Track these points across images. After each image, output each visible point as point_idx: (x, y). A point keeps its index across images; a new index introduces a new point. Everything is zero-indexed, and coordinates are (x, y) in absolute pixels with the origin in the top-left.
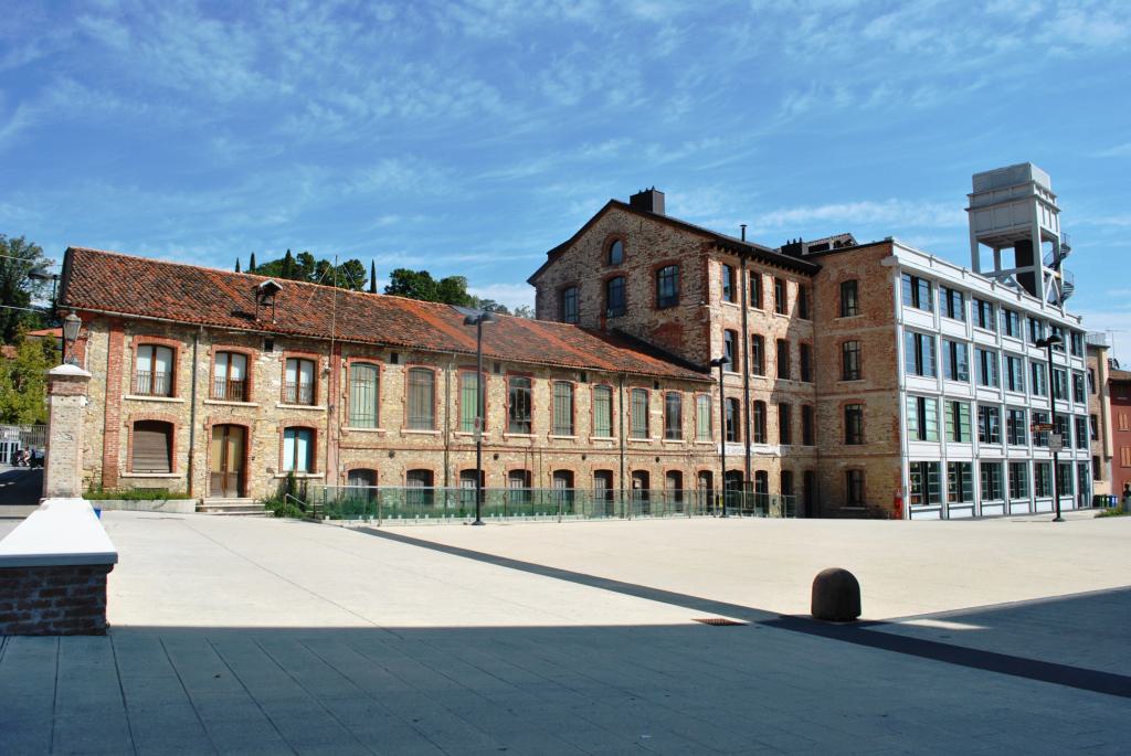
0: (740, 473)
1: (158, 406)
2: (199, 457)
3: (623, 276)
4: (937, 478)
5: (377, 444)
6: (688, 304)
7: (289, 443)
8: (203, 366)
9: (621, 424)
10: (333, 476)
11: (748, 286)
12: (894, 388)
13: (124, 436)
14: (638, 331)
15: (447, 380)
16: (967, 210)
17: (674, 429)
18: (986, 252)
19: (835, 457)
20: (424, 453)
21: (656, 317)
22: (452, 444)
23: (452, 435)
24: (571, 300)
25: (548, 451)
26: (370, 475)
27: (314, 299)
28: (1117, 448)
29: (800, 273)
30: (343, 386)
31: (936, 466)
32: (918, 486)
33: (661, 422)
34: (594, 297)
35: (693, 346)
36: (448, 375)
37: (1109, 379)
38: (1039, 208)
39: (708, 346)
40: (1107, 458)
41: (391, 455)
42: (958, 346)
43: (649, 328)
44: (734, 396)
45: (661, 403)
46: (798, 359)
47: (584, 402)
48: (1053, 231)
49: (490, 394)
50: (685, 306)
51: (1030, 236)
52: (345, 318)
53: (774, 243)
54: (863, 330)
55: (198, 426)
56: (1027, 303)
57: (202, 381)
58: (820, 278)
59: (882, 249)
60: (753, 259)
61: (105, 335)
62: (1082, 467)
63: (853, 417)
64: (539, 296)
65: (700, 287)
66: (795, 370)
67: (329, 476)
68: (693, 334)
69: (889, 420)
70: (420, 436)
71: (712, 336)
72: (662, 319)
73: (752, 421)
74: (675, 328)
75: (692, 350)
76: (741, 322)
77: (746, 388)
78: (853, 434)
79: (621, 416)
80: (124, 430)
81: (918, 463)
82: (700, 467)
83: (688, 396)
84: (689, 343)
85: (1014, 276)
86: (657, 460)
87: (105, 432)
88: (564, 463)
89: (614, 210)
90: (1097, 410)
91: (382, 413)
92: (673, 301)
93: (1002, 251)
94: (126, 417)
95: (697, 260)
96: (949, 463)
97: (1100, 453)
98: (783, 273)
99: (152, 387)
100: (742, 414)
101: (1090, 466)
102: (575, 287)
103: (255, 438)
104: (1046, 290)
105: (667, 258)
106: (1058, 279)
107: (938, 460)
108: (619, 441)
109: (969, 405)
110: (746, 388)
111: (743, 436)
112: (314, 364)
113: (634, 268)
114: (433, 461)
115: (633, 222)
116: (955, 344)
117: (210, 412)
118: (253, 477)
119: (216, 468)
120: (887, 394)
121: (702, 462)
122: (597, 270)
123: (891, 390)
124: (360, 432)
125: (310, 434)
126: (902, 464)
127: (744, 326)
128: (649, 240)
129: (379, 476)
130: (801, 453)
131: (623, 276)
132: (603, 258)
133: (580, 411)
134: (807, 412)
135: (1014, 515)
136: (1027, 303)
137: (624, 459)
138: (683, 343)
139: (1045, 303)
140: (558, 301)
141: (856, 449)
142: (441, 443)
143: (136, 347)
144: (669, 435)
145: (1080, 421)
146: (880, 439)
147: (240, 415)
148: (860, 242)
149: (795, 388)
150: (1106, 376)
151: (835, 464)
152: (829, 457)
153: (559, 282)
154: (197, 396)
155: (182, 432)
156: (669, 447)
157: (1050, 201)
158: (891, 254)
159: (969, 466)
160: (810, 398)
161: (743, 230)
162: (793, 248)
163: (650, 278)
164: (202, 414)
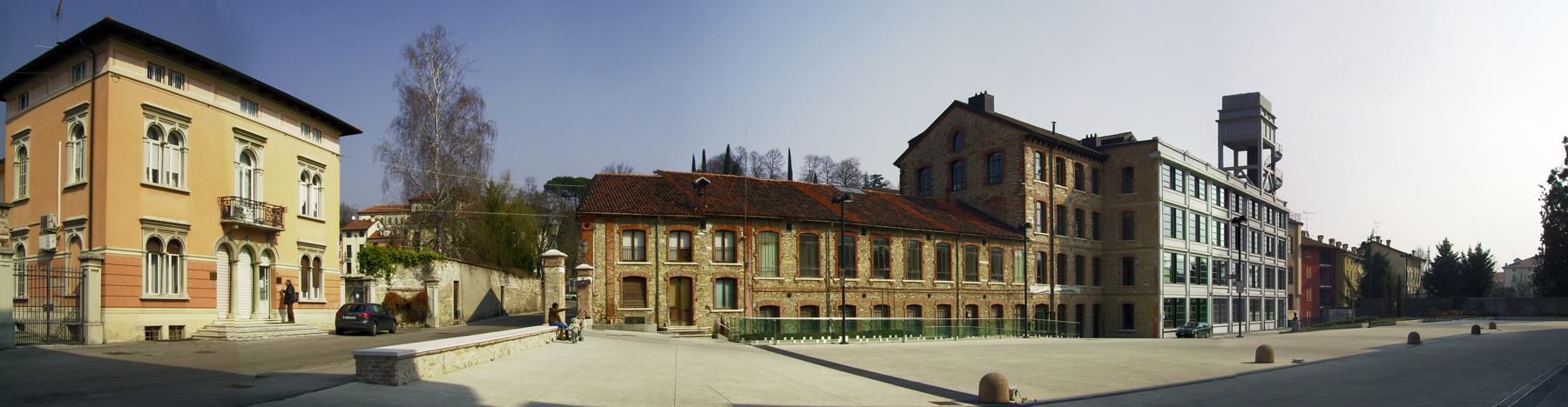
0: (1047, 306)
1: (636, 267)
2: (662, 297)
3: (963, 160)
5: (779, 288)
7: (719, 287)
8: (665, 242)
9: (957, 271)
10: (749, 311)
12: (1155, 246)
13: (617, 286)
15: (827, 242)
18: (1228, 153)
20: (812, 295)
22: (832, 287)
23: (831, 281)
26: (775, 310)
27: (735, 187)
28: (1304, 289)
29: (1094, 160)
30: (754, 248)
31: (1183, 301)
33: (987, 269)
36: (827, 238)
38: (1263, 125)
39: (1024, 213)
40: (1297, 296)
41: (789, 296)
44: (1043, 250)
45: (987, 255)
47: (929, 255)
48: (1272, 142)
49: (859, 251)
51: (1256, 143)
52: (755, 200)
53: (1079, 136)
54: (1138, 204)
55: (661, 279)
56: (1252, 191)
57: (662, 250)
60: (1059, 149)
61: (604, 226)
62: (1281, 302)
63: (1128, 265)
66: (1088, 231)
67: (747, 310)
69: (1152, 268)
70: (809, 282)
71: (1027, 207)
79: (957, 265)
80: (617, 283)
82: (1016, 302)
83: (1008, 249)
85: (1245, 171)
86: (984, 297)
87: (606, 284)
88: (914, 299)
89: (957, 109)
90: (1293, 264)
91: (781, 266)
93: (1239, 153)
94: (618, 275)
96: (1191, 299)
97: (1293, 293)
99: (633, 256)
100: (1048, 263)
103: (698, 285)
104: (1266, 185)
106: (1273, 175)
107: (1184, 297)
109: (1207, 259)
111: (1048, 280)
112: (734, 233)
113: (971, 154)
114: (819, 299)
115: (970, 119)
117: (668, 270)
118: (697, 312)
119: (673, 303)
121: (1017, 298)
122: (945, 155)
123: (1154, 247)
124: (766, 280)
125: (732, 282)
126: (1159, 298)
129: (781, 311)
131: (963, 160)
134: (1096, 261)
136: (1252, 191)
137: (960, 297)
139: (1263, 191)
141: (1129, 289)
142: (823, 287)
143: (621, 232)
144: (992, 278)
145: (1281, 272)
146: (1146, 282)
147: (686, 270)
148: (1138, 139)
149: (1088, 245)
150: (1300, 242)
152: (1110, 295)
154: (660, 260)
155: (651, 283)
156: (993, 288)
157: (1271, 121)
162: (1090, 141)
163: (983, 162)
164: (663, 271)
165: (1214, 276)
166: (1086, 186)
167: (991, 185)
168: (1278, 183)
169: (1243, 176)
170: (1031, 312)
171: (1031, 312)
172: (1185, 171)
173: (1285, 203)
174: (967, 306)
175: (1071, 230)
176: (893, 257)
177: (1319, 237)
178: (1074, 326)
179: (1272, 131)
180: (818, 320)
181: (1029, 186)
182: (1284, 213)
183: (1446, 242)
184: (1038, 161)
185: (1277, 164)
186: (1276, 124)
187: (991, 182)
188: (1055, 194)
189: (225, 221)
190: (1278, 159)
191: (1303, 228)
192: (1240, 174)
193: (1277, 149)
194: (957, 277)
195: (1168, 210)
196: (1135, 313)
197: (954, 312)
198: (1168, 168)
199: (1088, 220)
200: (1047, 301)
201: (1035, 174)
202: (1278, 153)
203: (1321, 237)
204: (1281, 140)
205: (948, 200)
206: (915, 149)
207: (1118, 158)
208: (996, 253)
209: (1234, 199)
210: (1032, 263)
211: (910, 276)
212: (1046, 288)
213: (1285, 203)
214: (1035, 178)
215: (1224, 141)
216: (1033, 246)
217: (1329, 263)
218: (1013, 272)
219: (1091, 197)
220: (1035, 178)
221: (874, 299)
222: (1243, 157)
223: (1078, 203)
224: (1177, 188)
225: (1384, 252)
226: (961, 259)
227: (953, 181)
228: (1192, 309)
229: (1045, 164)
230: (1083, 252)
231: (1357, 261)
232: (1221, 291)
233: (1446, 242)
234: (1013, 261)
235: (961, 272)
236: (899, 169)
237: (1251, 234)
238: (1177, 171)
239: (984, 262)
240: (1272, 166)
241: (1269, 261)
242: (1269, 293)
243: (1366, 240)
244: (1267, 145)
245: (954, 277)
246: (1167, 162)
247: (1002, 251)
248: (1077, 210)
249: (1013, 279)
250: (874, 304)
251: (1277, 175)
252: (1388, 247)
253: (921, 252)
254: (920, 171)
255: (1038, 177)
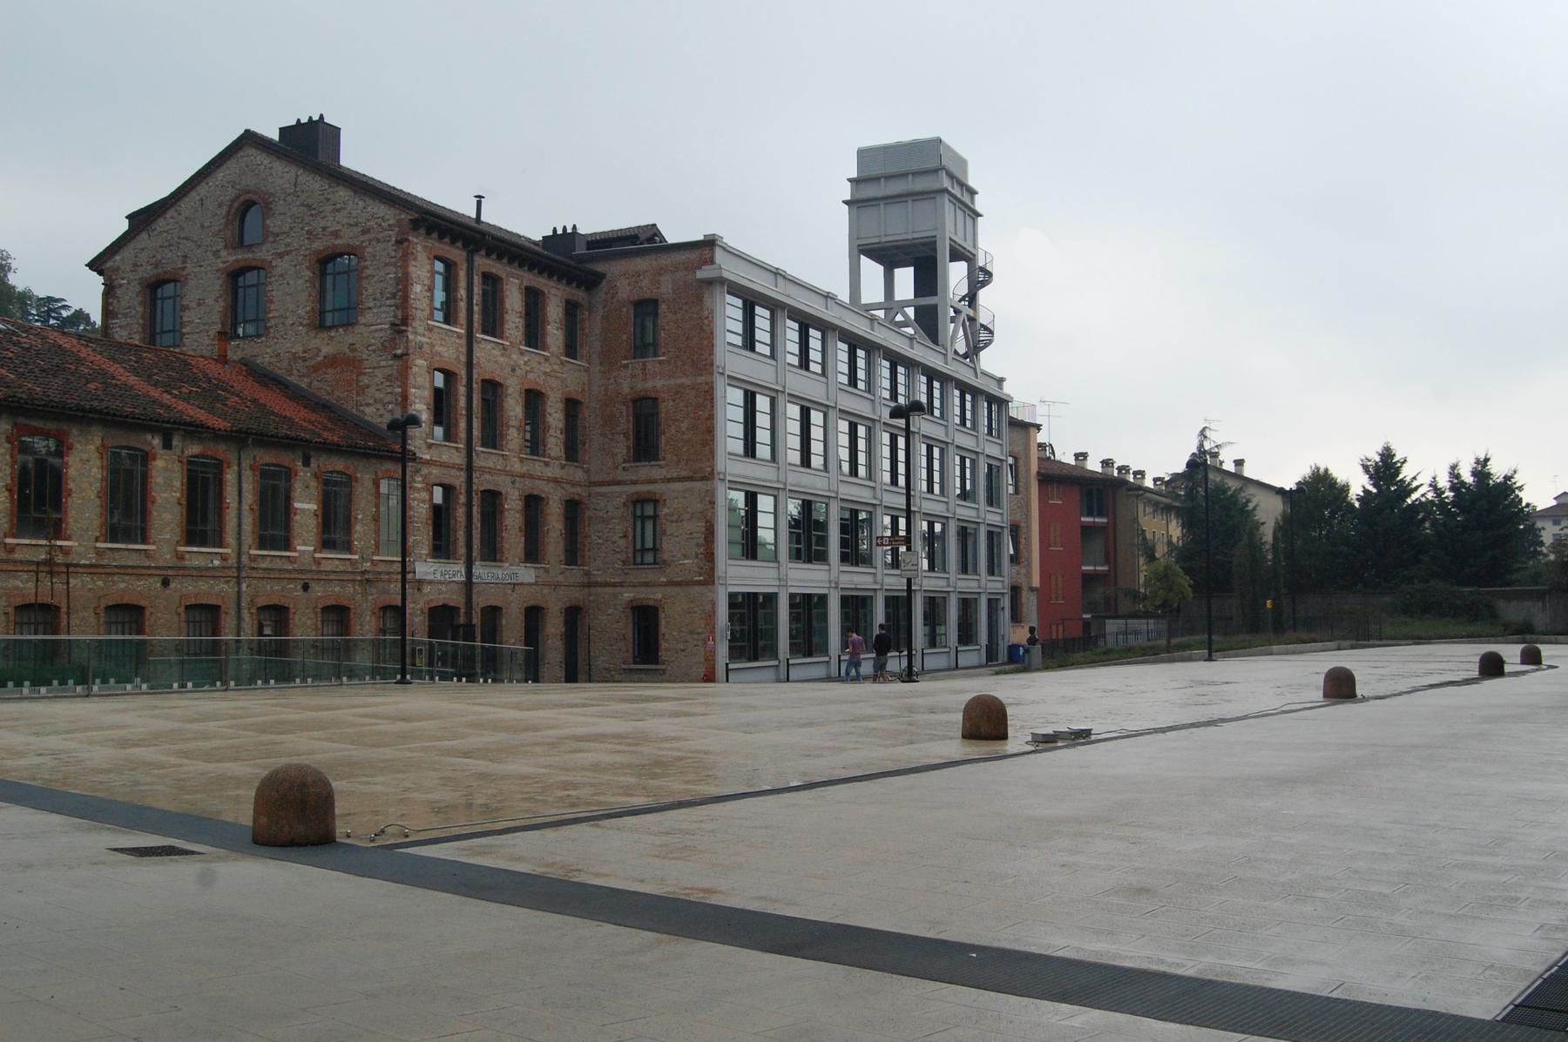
4: (773, 619)
6: (375, 321)
11: (477, 299)
14: (284, 364)
16: (846, 202)
17: (338, 536)
18: (872, 270)
19: (614, 585)
21: (315, 343)
24: (168, 304)
25: (93, 570)
29: (569, 283)
31: (771, 598)
32: (742, 631)
34: (210, 301)
35: (379, 395)
37: (1039, 473)
42: (813, 413)
43: (305, 360)
46: (561, 425)
50: (365, 325)
58: (601, 294)
59: (694, 255)
60: (488, 255)
64: (109, 293)
65: (394, 296)
66: (555, 443)
68: (380, 374)
69: (699, 526)
72: (325, 345)
73: (477, 523)
74: (347, 363)
75: (376, 401)
76: (463, 358)
77: (469, 469)
78: (645, 553)
79: (239, 509)
81: (743, 594)
83: (364, 476)
84: (372, 390)
85: (910, 312)
86: (306, 587)
89: (251, 151)
92: (349, 316)
95: (390, 248)
96: (792, 596)
98: (540, 282)
101: (1006, 602)
102: (175, 281)
105: (339, 242)
106: (972, 320)
108: (234, 555)
110: (469, 469)
113: (281, 256)
115: (281, 175)
116: (753, 395)
120: (697, 485)
123: (704, 478)
127: (470, 365)
128: (309, 207)
130: (561, 578)
132: (229, 234)
133: (159, 500)
134: (573, 509)
135: (792, 682)
137: (244, 586)
138: (362, 390)
139: (950, 355)
140: (142, 303)
144: (327, 544)
146: (686, 557)
148: (671, 238)
149: (554, 471)
151: (615, 596)
152: (606, 584)
153: (147, 271)
156: (327, 566)
157: (966, 199)
158: (712, 262)
159: (823, 598)
160: (579, 490)
161: (479, 204)
162: (562, 241)
163: (308, 273)
165: (844, 543)
166: (550, 340)
167: (330, 328)
168: (983, 336)
169: (905, 324)
170: (417, 620)
171: (417, 620)
172: (774, 306)
173: (1000, 381)
174: (262, 609)
175: (514, 437)
176: (71, 485)
177: (1077, 456)
178: (521, 657)
179: (969, 221)
180: (144, 641)
181: (417, 334)
182: (999, 403)
183: (1387, 454)
184: (439, 280)
185: (983, 295)
186: (978, 207)
187: (329, 322)
188: (478, 354)
189: (794, 641)
190: (984, 284)
191: (1041, 437)
192: (899, 318)
193: (981, 263)
194: (239, 539)
195: (736, 396)
196: (663, 629)
197: (228, 622)
198: (739, 302)
199: (555, 417)
200: (456, 599)
201: (433, 309)
202: (983, 269)
203: (1081, 456)
204: (990, 243)
205: (223, 359)
206: (144, 235)
207: (625, 279)
208: (336, 483)
209: (886, 373)
210: (420, 511)
211: (113, 533)
212: (456, 571)
213: (1000, 381)
214: (431, 316)
215: (865, 248)
216: (425, 471)
217: (1100, 515)
218: (377, 532)
219: (562, 363)
220: (431, 316)
221: (17, 588)
222: (905, 279)
223: (531, 376)
224: (759, 348)
225: (1233, 485)
226: (249, 498)
227: (236, 317)
228: (794, 618)
229: (456, 289)
230: (541, 488)
231: (1167, 509)
232: (857, 579)
233: (1387, 454)
234: (377, 506)
235: (248, 525)
236: (101, 279)
237: (924, 452)
238: (758, 310)
239: (306, 506)
240: (971, 298)
241: (966, 512)
242: (967, 584)
243: (1195, 451)
244: (957, 255)
245: (230, 538)
246: (735, 289)
247: (349, 480)
248: (528, 392)
249: (377, 546)
250: (19, 602)
251: (983, 319)
252: (1238, 476)
253: (145, 477)
254: (153, 287)
255: (439, 316)
